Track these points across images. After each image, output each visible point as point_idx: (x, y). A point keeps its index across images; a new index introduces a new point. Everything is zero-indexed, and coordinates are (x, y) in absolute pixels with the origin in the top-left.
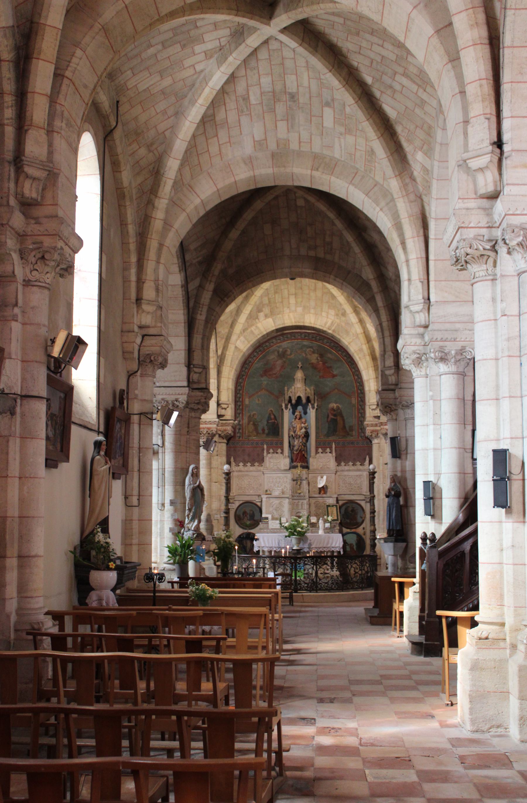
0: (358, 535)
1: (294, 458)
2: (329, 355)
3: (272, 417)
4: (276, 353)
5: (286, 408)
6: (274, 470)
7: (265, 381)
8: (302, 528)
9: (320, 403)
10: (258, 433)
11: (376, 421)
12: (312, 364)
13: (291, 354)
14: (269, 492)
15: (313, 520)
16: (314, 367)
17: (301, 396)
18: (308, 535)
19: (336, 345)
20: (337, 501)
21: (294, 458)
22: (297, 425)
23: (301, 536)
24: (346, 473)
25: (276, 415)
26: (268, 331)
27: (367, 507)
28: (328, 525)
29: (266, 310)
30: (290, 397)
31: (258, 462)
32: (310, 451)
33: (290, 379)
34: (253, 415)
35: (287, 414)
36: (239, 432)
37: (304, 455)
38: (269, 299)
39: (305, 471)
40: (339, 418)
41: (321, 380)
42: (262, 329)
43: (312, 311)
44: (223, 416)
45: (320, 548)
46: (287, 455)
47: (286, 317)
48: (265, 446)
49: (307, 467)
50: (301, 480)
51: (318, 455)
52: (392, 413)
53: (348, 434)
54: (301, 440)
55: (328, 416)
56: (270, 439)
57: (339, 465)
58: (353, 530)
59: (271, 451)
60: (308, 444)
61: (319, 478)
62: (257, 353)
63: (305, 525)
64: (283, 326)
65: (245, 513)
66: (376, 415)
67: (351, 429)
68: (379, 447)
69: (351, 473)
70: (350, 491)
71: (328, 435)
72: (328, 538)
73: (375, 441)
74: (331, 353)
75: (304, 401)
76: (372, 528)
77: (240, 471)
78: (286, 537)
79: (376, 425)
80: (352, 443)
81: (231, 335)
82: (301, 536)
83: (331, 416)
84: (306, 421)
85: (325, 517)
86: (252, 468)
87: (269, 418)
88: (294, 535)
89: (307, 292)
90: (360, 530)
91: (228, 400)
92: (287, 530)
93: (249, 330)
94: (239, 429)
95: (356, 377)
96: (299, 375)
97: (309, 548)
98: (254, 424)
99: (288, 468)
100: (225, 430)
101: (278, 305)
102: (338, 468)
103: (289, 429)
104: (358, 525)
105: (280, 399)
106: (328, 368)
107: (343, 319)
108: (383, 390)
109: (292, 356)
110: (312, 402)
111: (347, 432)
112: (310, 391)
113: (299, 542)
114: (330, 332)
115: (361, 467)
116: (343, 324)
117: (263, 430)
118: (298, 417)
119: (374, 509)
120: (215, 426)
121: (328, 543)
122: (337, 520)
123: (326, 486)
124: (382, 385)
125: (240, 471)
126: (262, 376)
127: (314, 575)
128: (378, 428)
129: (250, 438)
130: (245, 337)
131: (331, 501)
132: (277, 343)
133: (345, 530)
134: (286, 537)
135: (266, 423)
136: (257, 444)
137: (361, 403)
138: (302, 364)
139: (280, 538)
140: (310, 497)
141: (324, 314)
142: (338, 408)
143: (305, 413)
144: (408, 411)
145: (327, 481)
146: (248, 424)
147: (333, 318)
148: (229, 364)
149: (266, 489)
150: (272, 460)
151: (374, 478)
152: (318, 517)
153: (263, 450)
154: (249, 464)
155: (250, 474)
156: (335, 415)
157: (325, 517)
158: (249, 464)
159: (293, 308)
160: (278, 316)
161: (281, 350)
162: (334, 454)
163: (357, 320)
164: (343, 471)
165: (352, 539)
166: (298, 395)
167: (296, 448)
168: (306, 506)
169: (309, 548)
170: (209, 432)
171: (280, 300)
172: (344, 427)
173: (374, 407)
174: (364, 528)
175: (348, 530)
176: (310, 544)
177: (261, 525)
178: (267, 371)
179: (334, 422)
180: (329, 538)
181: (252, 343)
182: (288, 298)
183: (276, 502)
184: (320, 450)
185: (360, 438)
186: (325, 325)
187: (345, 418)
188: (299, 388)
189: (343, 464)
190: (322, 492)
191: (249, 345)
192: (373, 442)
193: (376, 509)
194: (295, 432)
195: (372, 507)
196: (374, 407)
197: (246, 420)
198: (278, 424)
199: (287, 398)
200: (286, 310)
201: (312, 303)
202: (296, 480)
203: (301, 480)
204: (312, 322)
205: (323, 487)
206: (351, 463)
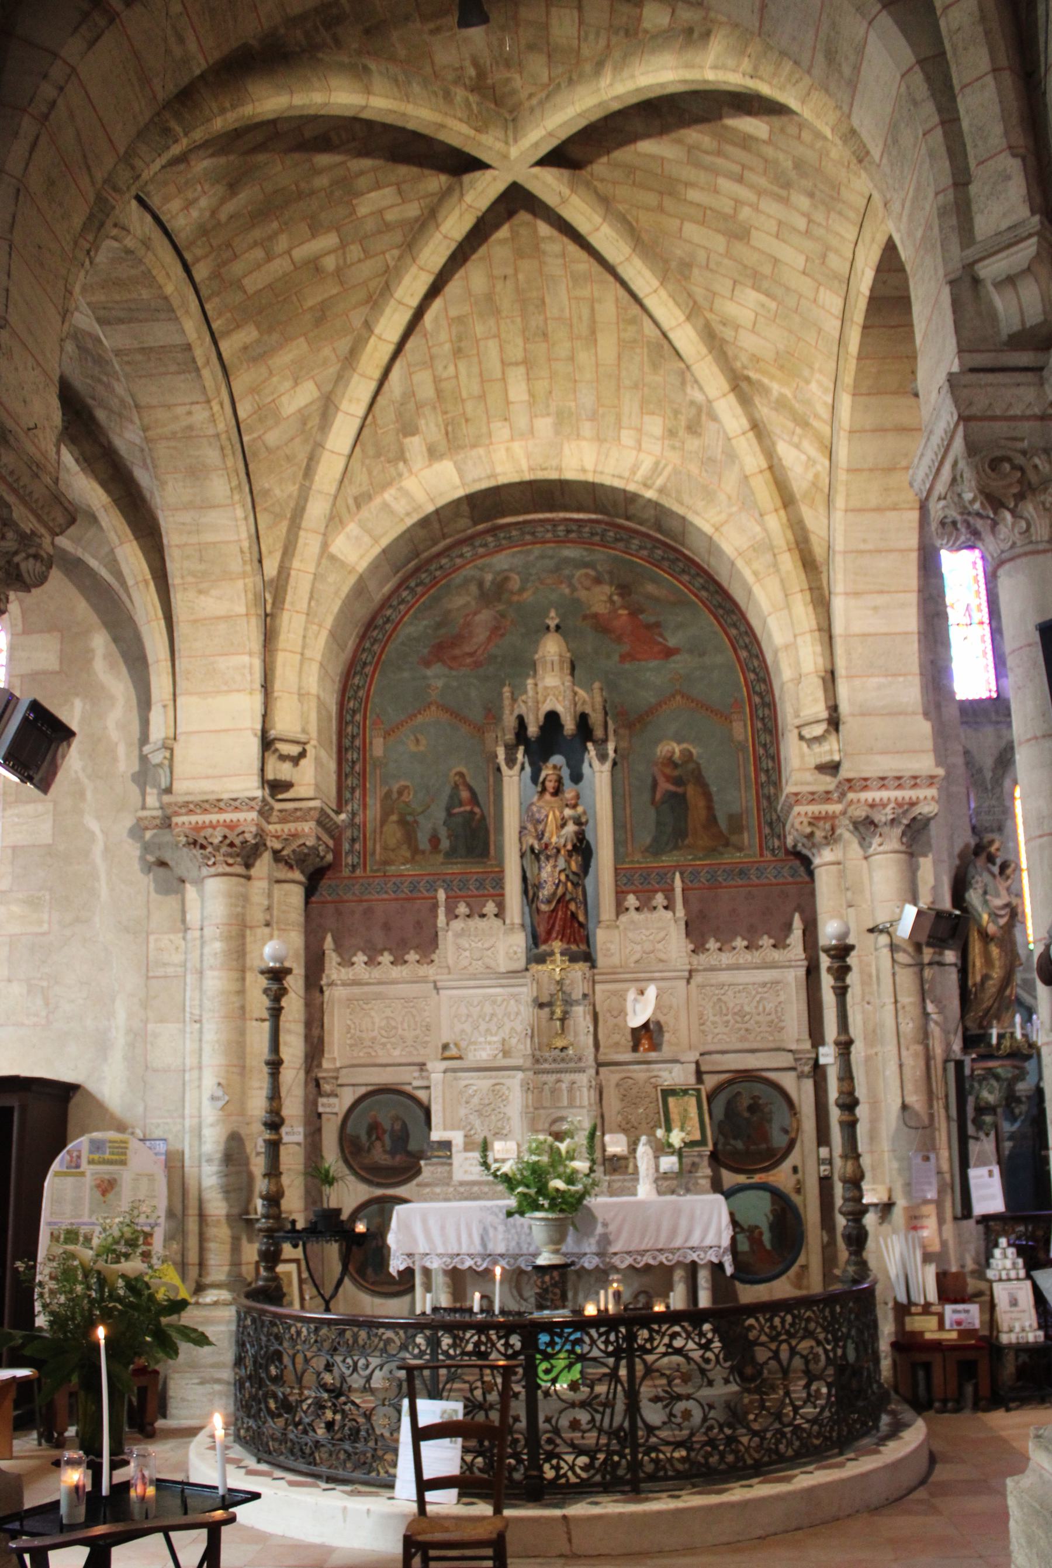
0: (777, 1194)
1: (541, 930)
2: (650, 588)
3: (465, 794)
4: (473, 588)
5: (511, 761)
6: (474, 977)
7: (437, 677)
8: (570, 1180)
9: (624, 744)
10: (416, 851)
11: (828, 783)
12: (595, 616)
13: (522, 590)
14: (453, 1051)
15: (615, 1144)
16: (601, 626)
17: (560, 709)
18: (597, 1202)
19: (672, 555)
20: (699, 1074)
21: (541, 930)
22: (550, 811)
23: (569, 1210)
24: (724, 977)
25: (477, 790)
26: (441, 502)
27: (804, 1094)
28: (669, 1163)
29: (431, 427)
30: (521, 720)
31: (417, 948)
32: (597, 906)
33: (524, 665)
34: (400, 793)
35: (514, 784)
36: (351, 851)
37: (574, 916)
38: (437, 381)
39: (579, 969)
40: (691, 791)
41: (627, 666)
42: (420, 497)
43: (587, 429)
44: (288, 786)
45: (643, 1253)
46: (517, 920)
47: (500, 454)
48: (441, 895)
49: (589, 958)
50: (568, 1002)
51: (624, 918)
52: (1029, 509)
53: (727, 844)
54: (561, 863)
55: (655, 785)
56: (456, 869)
57: (699, 948)
58: (757, 1178)
59: (462, 909)
60: (589, 881)
61: (631, 995)
62: (412, 590)
63: (581, 1165)
64: (492, 483)
65: (374, 1128)
66: (826, 759)
67: (736, 824)
68: (842, 875)
69: (743, 977)
70: (742, 1039)
71: (656, 849)
72: (674, 1216)
73: (824, 858)
74: (655, 580)
75: (569, 725)
76: (850, 1166)
77: (356, 983)
78: (510, 1214)
79: (827, 797)
80: (742, 873)
81: (306, 500)
82: (569, 1210)
83: (664, 786)
84: (578, 797)
85: (660, 1133)
86: (396, 972)
87: (454, 800)
88: (538, 1208)
89: (563, 349)
90: (781, 1177)
91: (304, 731)
92: (512, 1189)
93: (377, 501)
94: (353, 840)
95: (744, 654)
96: (552, 648)
97: (601, 1254)
98: (402, 822)
99: (521, 964)
100: (295, 836)
101: (469, 407)
102: (695, 960)
103: (523, 829)
104: (775, 1158)
105: (489, 736)
106: (648, 627)
107: (693, 444)
108: (962, 372)
109: (527, 596)
110: (599, 733)
111: (721, 836)
112: (591, 700)
113: (558, 1235)
114: (650, 494)
115: (776, 955)
116: (694, 468)
117: (435, 841)
118: (550, 785)
119: (851, 1093)
120: (253, 815)
121: (673, 1233)
122: (702, 1142)
123: (658, 1024)
124: (961, 351)
125: (356, 983)
126: (428, 664)
127: (620, 1406)
128: (836, 808)
129: (392, 869)
130: (362, 526)
131: (679, 1075)
132: (477, 557)
133: (730, 1178)
134: (510, 1214)
135: (442, 815)
136: (414, 888)
137: (765, 738)
138: (563, 617)
139: (490, 1219)
140: (599, 1065)
141: (627, 437)
142: (688, 756)
143: (577, 777)
145: (658, 1007)
146: (383, 822)
147: (657, 448)
148: (304, 606)
149: (444, 1041)
150: (464, 942)
151: (847, 969)
152: (632, 1132)
153: (435, 906)
154: (386, 958)
155: (392, 990)
156: (679, 781)
157: (660, 1133)
158: (386, 958)
159: (521, 421)
160: (474, 453)
161: (489, 577)
162: (680, 912)
163: (745, 423)
164: (712, 969)
165: (758, 1210)
166: (546, 707)
167: (545, 893)
168: (586, 1096)
169: (601, 1254)
170: (232, 837)
171: (476, 389)
172: (712, 820)
173: (819, 730)
174: (795, 1170)
175: (742, 1179)
176: (605, 1240)
177: (428, 1170)
178: (443, 648)
179: (677, 803)
180: (677, 1212)
181: (385, 542)
182: (504, 379)
183: (481, 1083)
184: (631, 900)
185: (768, 856)
186: (634, 472)
187: (714, 789)
188: (551, 689)
189: (712, 944)
190: (645, 1043)
191: (377, 550)
192: (817, 861)
193: (861, 1092)
194: (540, 837)
195: (846, 1087)
196: (819, 730)
197: (374, 810)
198: (483, 818)
199: (509, 722)
200: (501, 431)
201: (587, 398)
202: (550, 1004)
203: (568, 1002)
204: (589, 466)
205: (646, 1026)
206: (740, 943)
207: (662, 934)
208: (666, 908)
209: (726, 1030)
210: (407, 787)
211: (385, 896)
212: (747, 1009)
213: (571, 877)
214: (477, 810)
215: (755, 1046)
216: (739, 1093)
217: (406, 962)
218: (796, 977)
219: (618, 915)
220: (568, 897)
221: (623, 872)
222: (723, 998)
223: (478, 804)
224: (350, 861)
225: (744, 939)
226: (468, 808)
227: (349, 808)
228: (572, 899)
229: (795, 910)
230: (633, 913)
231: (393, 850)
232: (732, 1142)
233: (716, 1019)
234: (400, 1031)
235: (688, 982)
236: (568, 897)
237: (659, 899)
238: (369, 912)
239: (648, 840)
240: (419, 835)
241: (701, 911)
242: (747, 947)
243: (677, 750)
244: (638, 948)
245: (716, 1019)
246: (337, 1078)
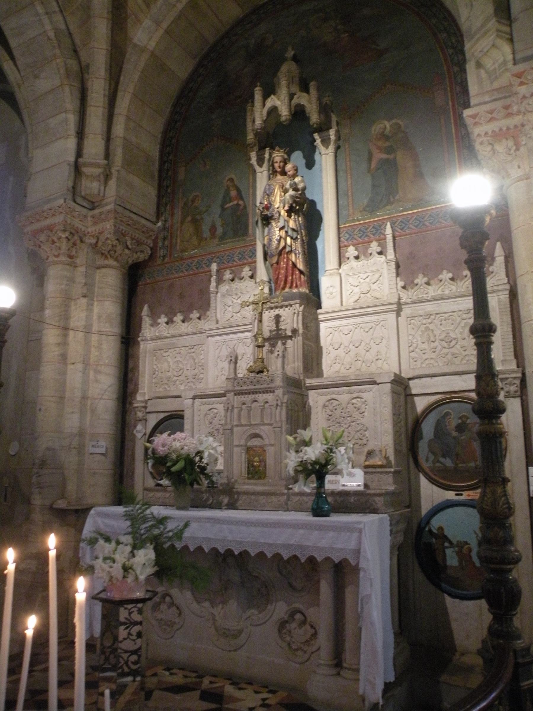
3: (233, 193)
31: (198, 309)
94: (165, 239)
117: (213, 229)
144: (23, 566)
184: (351, 251)
198: (245, 207)
207: (377, 276)
208: (380, 253)
209: (434, 356)
210: (197, 196)
211: (182, 274)
212: (453, 335)
213: (290, 232)
214: (241, 202)
215: (461, 369)
216: (447, 414)
217: (191, 319)
218: (499, 302)
219: (340, 265)
220: (288, 249)
221: (345, 230)
222: (431, 327)
223: (241, 198)
224: (162, 254)
225: (449, 271)
226: (235, 202)
227: (163, 218)
228: (291, 251)
229: (498, 240)
230: (354, 263)
231: (188, 241)
232: (442, 459)
233: (425, 346)
234: (185, 372)
235: (398, 315)
236: (288, 249)
237: (374, 247)
238: (171, 286)
239: (366, 202)
240: (204, 227)
241: (411, 253)
242: (452, 279)
243: (388, 126)
244: (357, 290)
245: (425, 346)
246: (146, 407)
